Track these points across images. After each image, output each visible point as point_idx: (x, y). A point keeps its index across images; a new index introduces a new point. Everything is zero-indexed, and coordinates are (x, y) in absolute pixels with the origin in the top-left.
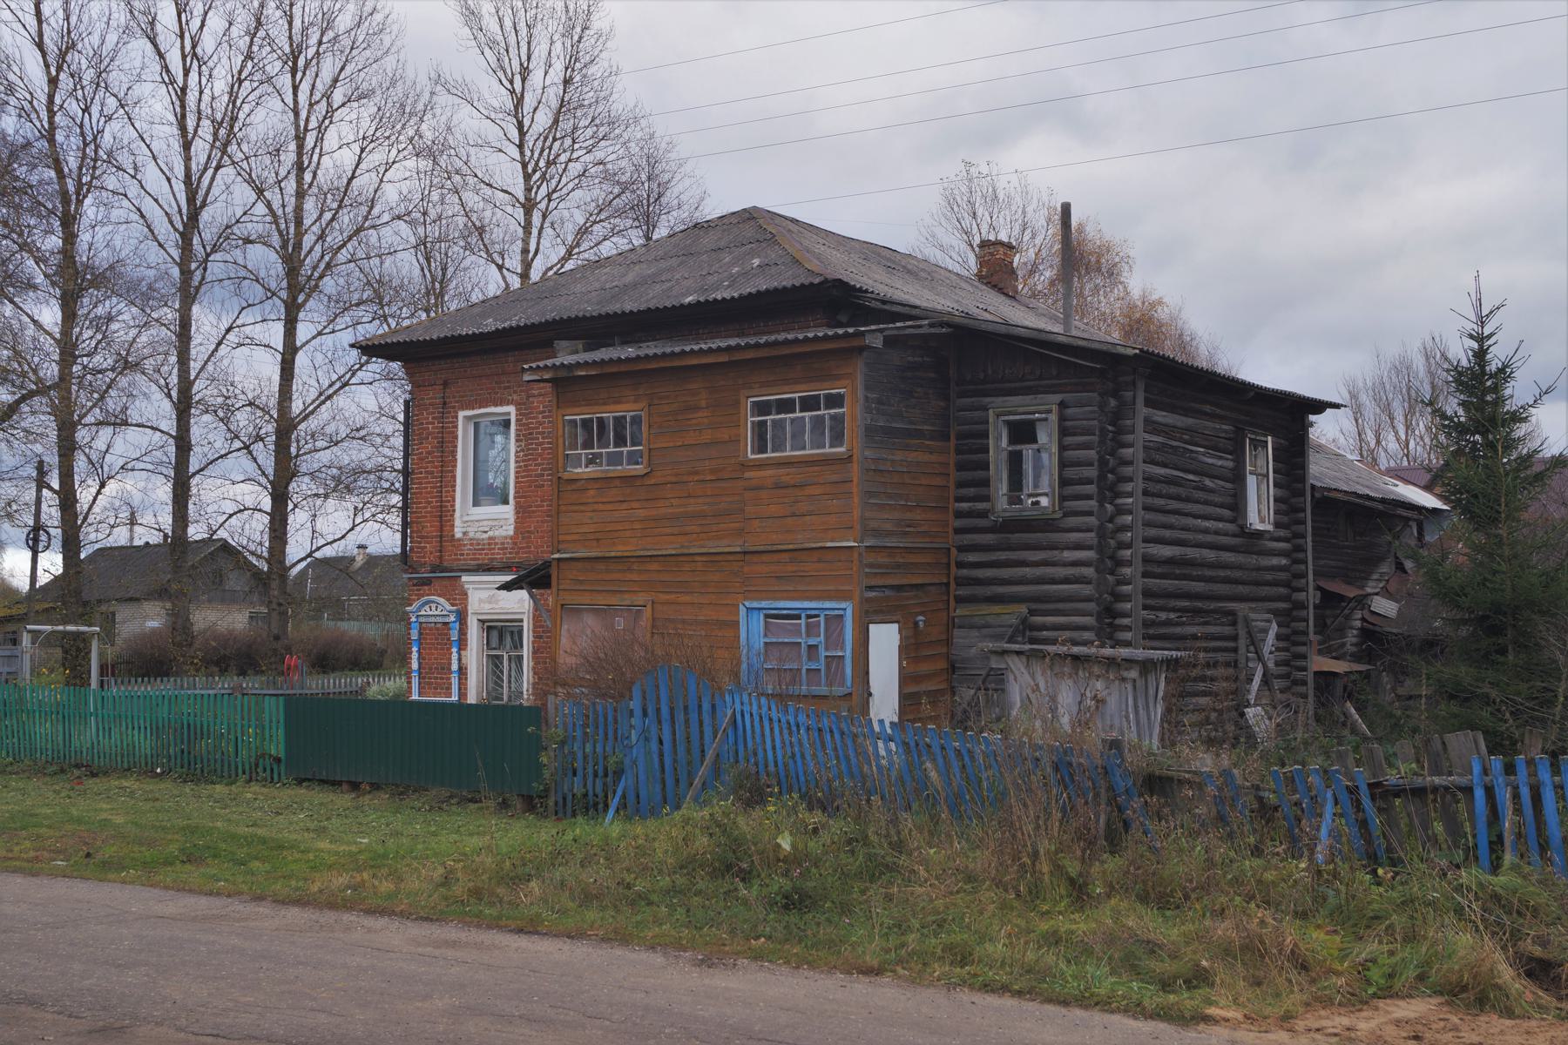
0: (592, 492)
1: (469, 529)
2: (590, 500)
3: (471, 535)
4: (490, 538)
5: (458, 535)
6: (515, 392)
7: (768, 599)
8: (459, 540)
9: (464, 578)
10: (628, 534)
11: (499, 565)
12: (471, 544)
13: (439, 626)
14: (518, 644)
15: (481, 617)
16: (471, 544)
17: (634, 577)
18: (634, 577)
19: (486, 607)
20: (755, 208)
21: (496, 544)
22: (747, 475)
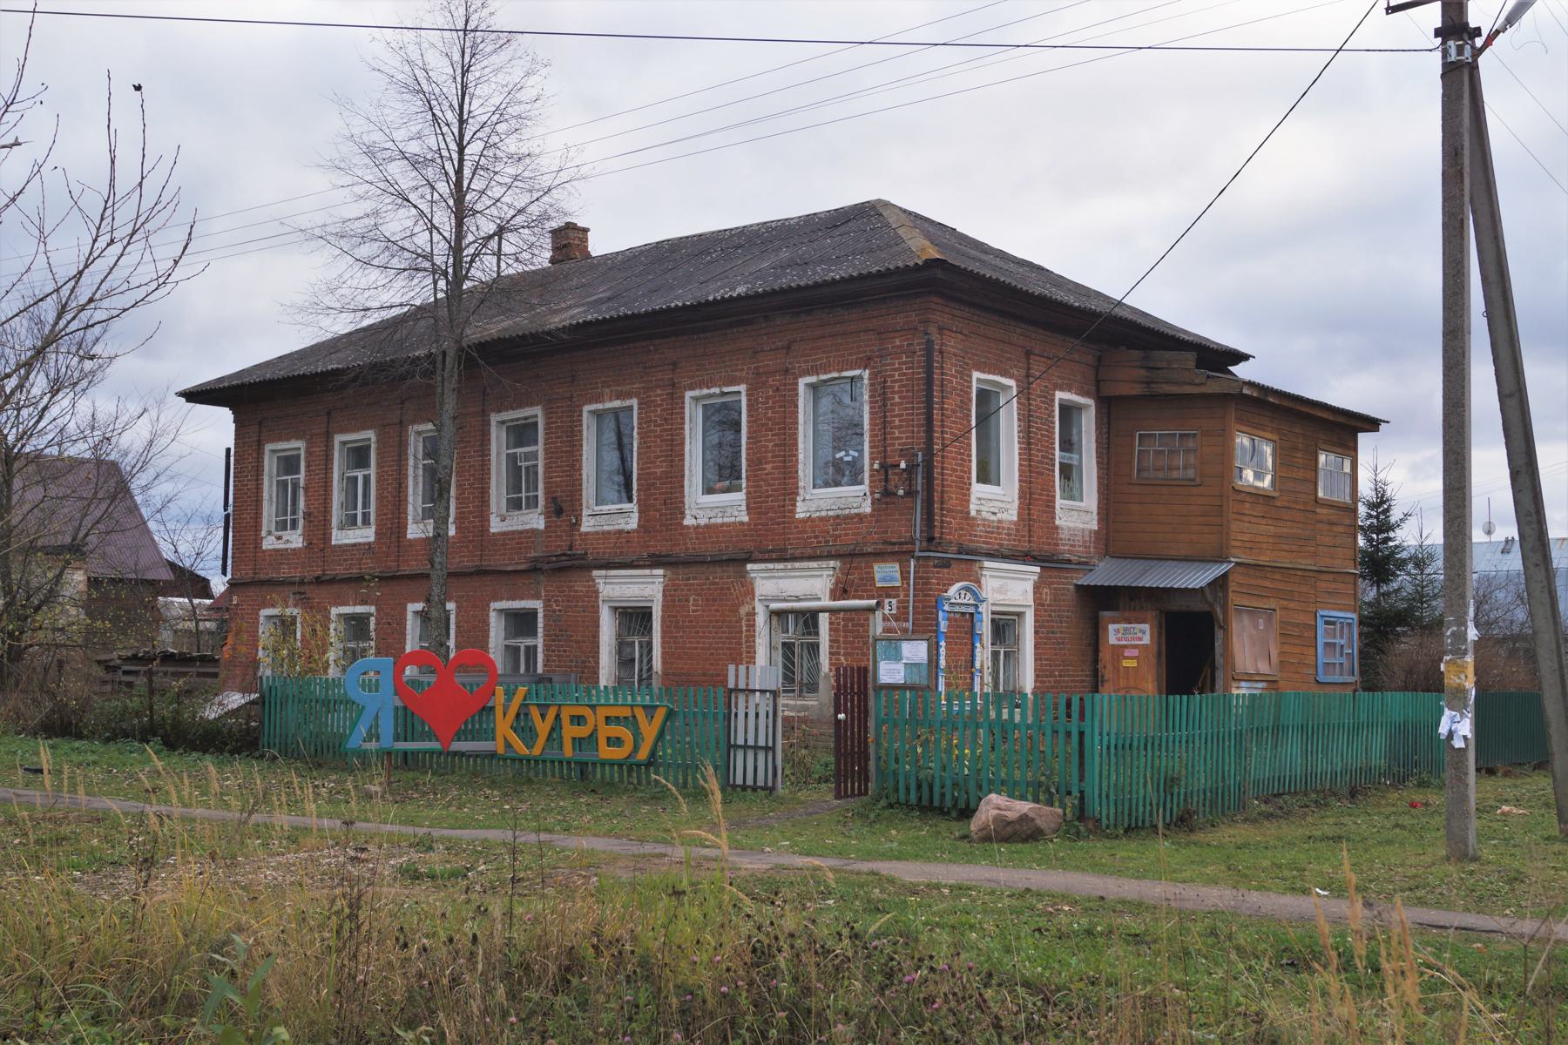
0: (1247, 505)
1: (982, 508)
2: (1247, 512)
3: (984, 515)
4: (1000, 521)
5: (973, 513)
6: (1015, 366)
7: (1328, 609)
8: (974, 519)
9: (987, 564)
10: (1265, 546)
11: (1007, 552)
12: (984, 525)
13: (958, 616)
14: (648, 630)
15: (774, 606)
16: (984, 525)
17: (1268, 584)
18: (1268, 584)
19: (999, 598)
20: (879, 201)
21: (1003, 528)
22: (1318, 510)
